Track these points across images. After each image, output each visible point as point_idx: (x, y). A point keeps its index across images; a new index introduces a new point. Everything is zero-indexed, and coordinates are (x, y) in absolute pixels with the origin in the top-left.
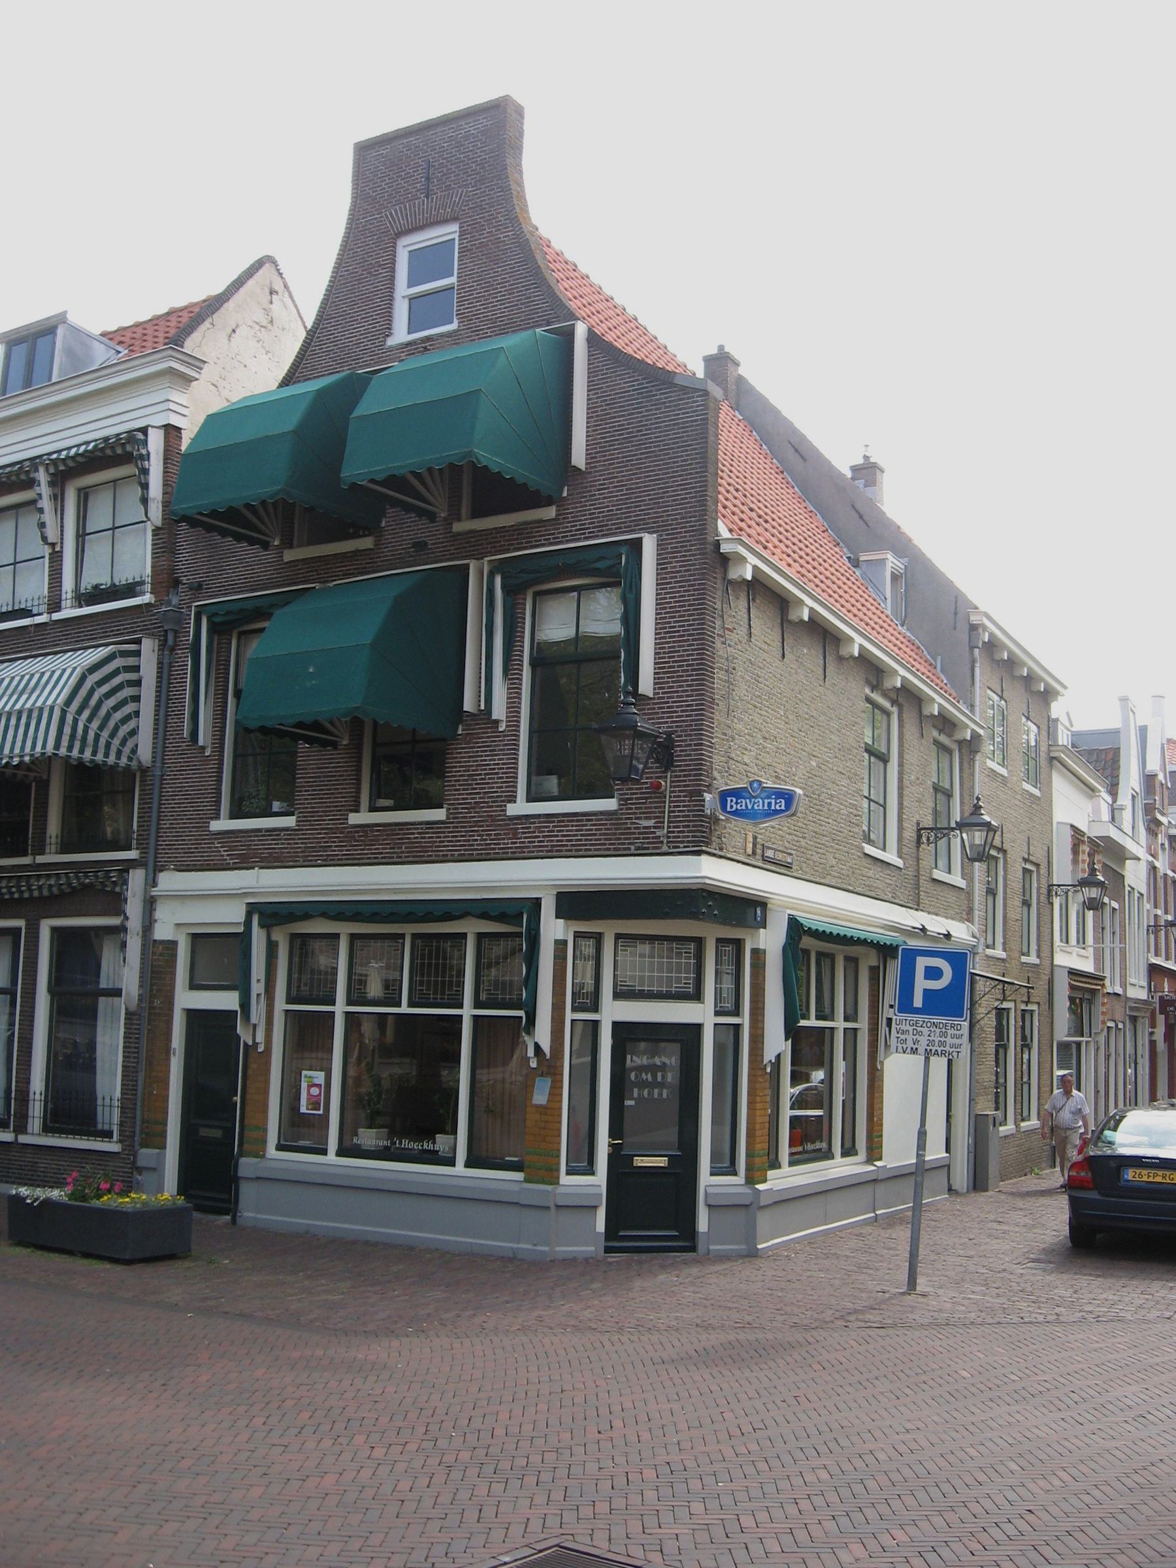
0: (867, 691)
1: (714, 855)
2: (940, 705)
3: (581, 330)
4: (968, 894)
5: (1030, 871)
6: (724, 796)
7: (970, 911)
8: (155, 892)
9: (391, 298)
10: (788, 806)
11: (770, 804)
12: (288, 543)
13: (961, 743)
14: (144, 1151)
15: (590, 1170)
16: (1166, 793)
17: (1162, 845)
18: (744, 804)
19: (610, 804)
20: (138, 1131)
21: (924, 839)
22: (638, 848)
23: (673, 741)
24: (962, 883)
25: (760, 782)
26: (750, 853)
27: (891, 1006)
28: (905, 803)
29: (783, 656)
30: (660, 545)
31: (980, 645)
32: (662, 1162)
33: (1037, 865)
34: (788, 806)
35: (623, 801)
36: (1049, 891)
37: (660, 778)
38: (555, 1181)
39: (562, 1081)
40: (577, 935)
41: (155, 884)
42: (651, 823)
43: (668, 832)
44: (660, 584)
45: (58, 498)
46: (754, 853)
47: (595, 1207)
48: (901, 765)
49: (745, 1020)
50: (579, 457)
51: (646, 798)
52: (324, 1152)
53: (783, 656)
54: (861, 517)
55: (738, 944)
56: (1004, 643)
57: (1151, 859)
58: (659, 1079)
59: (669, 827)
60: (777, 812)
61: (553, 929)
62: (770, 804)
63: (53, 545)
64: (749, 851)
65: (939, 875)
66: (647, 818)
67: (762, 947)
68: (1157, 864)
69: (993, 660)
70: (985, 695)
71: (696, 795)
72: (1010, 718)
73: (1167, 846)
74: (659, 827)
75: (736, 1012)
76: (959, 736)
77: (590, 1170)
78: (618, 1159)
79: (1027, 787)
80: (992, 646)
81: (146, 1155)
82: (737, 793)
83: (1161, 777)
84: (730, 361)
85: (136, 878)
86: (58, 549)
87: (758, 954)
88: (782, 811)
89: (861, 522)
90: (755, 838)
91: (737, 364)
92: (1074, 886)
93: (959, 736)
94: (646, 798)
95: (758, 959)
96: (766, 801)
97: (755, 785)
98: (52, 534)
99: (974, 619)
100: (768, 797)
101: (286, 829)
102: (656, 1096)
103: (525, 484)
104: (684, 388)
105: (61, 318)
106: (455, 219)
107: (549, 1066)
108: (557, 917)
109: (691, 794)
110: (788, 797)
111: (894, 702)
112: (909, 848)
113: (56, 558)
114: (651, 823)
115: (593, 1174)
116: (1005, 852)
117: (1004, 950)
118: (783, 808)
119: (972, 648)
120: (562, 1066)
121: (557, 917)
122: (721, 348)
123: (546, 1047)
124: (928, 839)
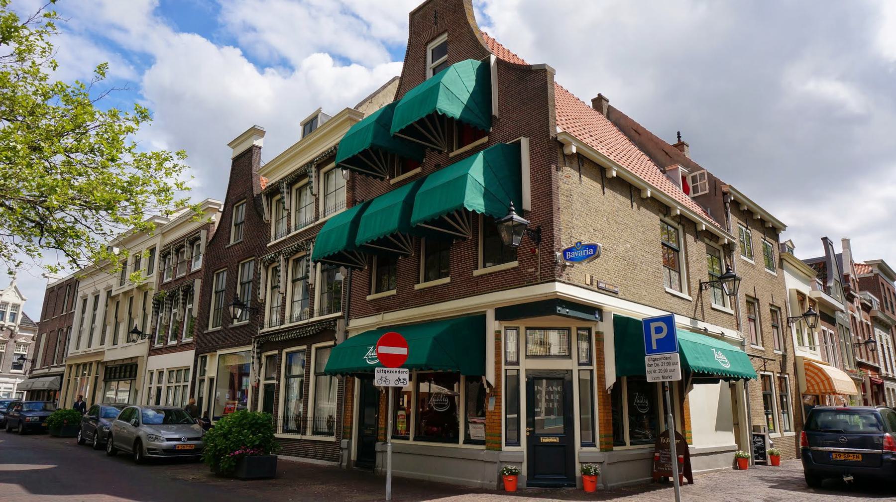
0: (662, 217)
1: (564, 282)
2: (705, 225)
3: (493, 58)
4: (737, 318)
5: (776, 312)
6: (565, 252)
7: (738, 325)
8: (348, 328)
9: (425, 69)
10: (594, 252)
11: (586, 252)
12: (392, 177)
13: (724, 246)
14: (343, 440)
15: (518, 444)
16: (857, 284)
17: (857, 307)
18: (574, 254)
19: (515, 264)
20: (342, 432)
21: (704, 288)
22: (528, 283)
23: (541, 230)
24: (732, 312)
25: (580, 243)
26: (589, 284)
27: (101, 70)
28: (690, 271)
29: (604, 193)
30: (531, 143)
31: (729, 201)
32: (555, 440)
33: (780, 308)
34: (594, 252)
35: (521, 262)
36: (788, 321)
37: (536, 248)
38: (500, 449)
39: (501, 399)
40: (506, 328)
41: (348, 325)
42: (533, 270)
43: (541, 273)
44: (532, 159)
45: (290, 193)
46: (592, 284)
47: (521, 463)
48: (686, 253)
49: (595, 367)
50: (495, 111)
51: (530, 259)
52: (408, 439)
53: (604, 193)
54: (667, 154)
55: (589, 330)
56: (743, 201)
57: (851, 313)
58: (552, 398)
59: (541, 270)
60: (589, 256)
61: (493, 326)
62: (586, 252)
63: (315, 195)
64: (588, 282)
65: (714, 306)
66: (531, 268)
67: (601, 330)
68: (855, 315)
69: (740, 211)
70: (734, 221)
71: (552, 253)
72: (753, 238)
73: (860, 307)
74: (537, 271)
75: (591, 364)
76: (721, 242)
77: (518, 444)
78: (532, 439)
79: (766, 270)
80: (736, 204)
81: (344, 443)
82: (570, 250)
83: (852, 276)
84: (603, 101)
85: (341, 323)
86: (317, 197)
87: (599, 335)
88: (591, 255)
89: (668, 156)
90: (592, 277)
91: (608, 101)
92: (801, 317)
93: (721, 242)
94: (530, 259)
95: (599, 336)
96: (584, 251)
97: (578, 244)
98: (315, 192)
99: (725, 189)
100: (585, 249)
101: (393, 295)
102: (551, 406)
103: (468, 124)
104: (536, 71)
105: (319, 110)
106: (446, 31)
107: (496, 392)
108: (496, 320)
109: (550, 253)
110: (594, 247)
111: (679, 223)
112: (695, 292)
113: (317, 200)
114: (533, 270)
115: (519, 445)
116: (758, 300)
117: (763, 346)
118: (592, 253)
119: (725, 203)
120: (501, 392)
121: (496, 320)
122: (599, 95)
123: (492, 382)
124: (706, 287)
